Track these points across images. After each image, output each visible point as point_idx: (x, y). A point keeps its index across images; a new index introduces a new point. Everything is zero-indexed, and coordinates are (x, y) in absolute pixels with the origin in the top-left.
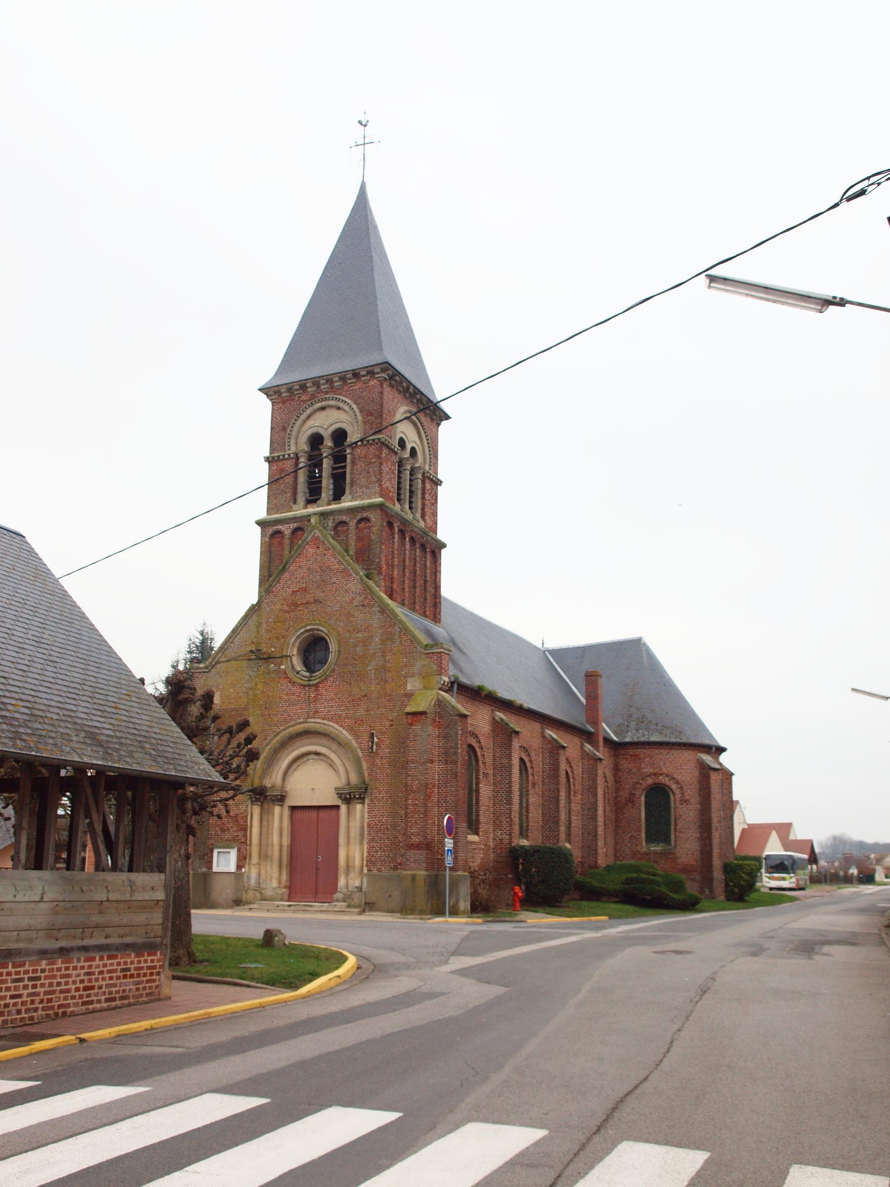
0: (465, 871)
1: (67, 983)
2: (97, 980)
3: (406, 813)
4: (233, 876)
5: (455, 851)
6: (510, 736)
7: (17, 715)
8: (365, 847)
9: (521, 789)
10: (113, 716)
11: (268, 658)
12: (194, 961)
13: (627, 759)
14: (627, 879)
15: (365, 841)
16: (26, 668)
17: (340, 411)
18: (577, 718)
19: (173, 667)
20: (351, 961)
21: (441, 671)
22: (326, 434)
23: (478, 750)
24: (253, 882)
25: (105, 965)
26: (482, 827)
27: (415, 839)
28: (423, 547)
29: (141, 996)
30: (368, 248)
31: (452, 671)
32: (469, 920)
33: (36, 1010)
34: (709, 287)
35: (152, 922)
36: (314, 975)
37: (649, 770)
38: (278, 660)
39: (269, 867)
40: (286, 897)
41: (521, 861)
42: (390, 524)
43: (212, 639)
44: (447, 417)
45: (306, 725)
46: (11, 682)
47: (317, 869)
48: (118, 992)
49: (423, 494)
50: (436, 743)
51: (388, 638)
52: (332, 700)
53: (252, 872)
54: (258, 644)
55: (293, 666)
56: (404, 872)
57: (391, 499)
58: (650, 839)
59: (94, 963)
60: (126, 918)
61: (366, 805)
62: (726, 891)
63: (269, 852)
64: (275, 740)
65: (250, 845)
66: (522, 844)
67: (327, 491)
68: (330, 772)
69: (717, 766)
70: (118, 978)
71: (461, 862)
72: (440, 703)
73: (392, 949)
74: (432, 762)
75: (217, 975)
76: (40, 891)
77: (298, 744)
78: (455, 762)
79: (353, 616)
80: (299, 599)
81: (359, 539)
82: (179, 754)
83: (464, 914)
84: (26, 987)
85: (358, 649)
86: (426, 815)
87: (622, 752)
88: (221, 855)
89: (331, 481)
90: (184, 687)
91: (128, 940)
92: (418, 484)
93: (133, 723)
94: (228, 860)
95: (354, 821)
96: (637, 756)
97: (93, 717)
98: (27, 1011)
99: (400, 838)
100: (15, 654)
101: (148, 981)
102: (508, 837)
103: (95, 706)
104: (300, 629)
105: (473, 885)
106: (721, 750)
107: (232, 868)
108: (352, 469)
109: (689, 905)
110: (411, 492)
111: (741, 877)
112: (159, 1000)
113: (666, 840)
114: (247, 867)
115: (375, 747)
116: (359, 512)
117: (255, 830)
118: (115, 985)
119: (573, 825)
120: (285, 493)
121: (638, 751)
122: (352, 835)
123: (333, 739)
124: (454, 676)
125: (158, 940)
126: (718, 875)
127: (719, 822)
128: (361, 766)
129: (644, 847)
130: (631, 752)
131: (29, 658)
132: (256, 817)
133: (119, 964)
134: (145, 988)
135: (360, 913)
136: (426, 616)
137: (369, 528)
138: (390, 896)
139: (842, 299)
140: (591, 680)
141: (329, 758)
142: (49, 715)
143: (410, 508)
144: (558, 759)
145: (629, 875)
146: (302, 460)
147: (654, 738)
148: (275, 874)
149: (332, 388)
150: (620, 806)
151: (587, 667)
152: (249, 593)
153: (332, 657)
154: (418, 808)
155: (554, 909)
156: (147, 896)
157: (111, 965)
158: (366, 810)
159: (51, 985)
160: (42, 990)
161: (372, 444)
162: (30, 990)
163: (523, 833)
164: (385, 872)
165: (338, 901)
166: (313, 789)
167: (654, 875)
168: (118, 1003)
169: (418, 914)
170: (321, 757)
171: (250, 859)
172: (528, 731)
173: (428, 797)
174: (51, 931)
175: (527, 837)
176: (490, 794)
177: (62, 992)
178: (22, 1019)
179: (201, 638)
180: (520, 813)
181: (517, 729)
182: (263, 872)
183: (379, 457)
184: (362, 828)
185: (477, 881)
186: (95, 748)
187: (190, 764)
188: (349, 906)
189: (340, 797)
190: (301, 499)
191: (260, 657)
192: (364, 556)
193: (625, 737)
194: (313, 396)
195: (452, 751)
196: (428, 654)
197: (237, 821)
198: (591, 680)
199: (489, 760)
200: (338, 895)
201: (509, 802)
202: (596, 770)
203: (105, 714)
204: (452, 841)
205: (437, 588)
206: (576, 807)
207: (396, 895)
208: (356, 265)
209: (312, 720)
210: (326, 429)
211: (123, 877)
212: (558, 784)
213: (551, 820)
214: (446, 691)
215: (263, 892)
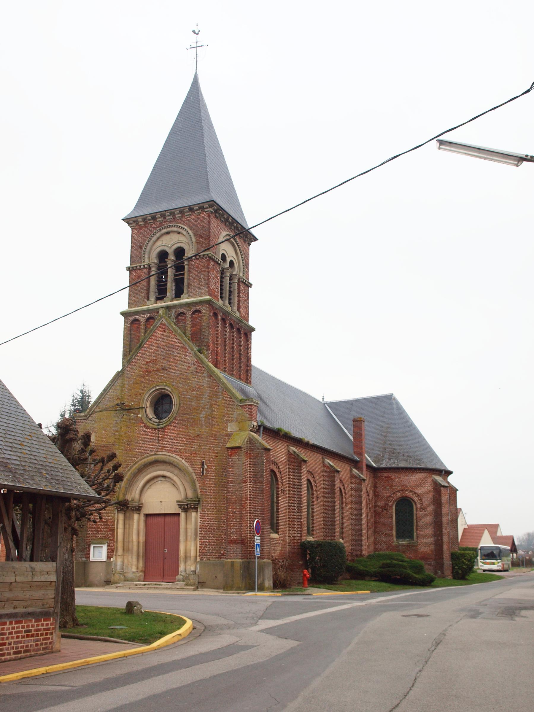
0: (269, 559)
3: (227, 519)
6: (300, 464)
8: (198, 542)
9: (308, 501)
10: (19, 451)
11: (129, 409)
12: (77, 625)
15: (198, 538)
17: (180, 235)
18: (347, 451)
19: (62, 416)
20: (189, 624)
21: (251, 417)
22: (170, 251)
23: (278, 474)
25: (13, 628)
26: (281, 528)
27: (234, 537)
28: (239, 330)
29: (39, 649)
30: (200, 121)
31: (259, 418)
34: (439, 148)
35: (47, 597)
36: (163, 634)
38: (136, 411)
40: (142, 579)
41: (308, 552)
42: (215, 315)
43: (89, 396)
44: (256, 239)
45: (156, 457)
47: (164, 558)
49: (239, 293)
50: (248, 468)
51: (214, 395)
52: (174, 438)
53: (118, 561)
54: (122, 399)
55: (147, 415)
57: (216, 297)
58: (398, 536)
60: (28, 594)
61: (199, 513)
62: (452, 573)
63: (130, 547)
64: (134, 467)
65: (117, 542)
66: (309, 540)
68: (174, 489)
69: (446, 485)
70: (23, 637)
71: (266, 553)
73: (217, 615)
74: (245, 482)
77: (151, 470)
78: (262, 482)
80: (152, 368)
81: (194, 325)
82: (67, 478)
83: (268, 589)
87: (379, 475)
88: (96, 549)
89: (174, 284)
90: (70, 430)
91: (30, 610)
92: (236, 286)
94: (101, 553)
95: (190, 525)
96: (390, 477)
97: (5, 452)
99: (223, 536)
101: (44, 639)
102: (299, 535)
105: (274, 569)
106: (449, 473)
107: (104, 558)
108: (189, 276)
110: (230, 292)
111: (463, 563)
112: (52, 652)
113: (411, 537)
114: (114, 557)
115: (205, 472)
116: (194, 306)
117: (120, 531)
118: (20, 642)
119: (345, 526)
123: (175, 466)
125: (51, 610)
126: (447, 561)
128: (195, 486)
129: (395, 541)
134: (42, 644)
135: (194, 590)
140: (357, 423)
141: (172, 480)
143: (230, 303)
144: (334, 479)
145: (384, 561)
148: (135, 562)
149: (174, 218)
150: (377, 513)
151: (354, 415)
152: (116, 364)
153: (174, 408)
154: (236, 515)
156: (43, 579)
157: (18, 628)
158: (199, 516)
161: (202, 258)
163: (310, 532)
164: (213, 560)
165: (179, 581)
166: (161, 502)
167: (402, 561)
168: (23, 655)
169: (236, 590)
170: (167, 479)
172: (313, 461)
173: (242, 507)
175: (312, 535)
176: (286, 505)
179: (81, 395)
180: (308, 518)
182: (126, 561)
183: (208, 268)
184: (196, 530)
185: (278, 566)
186: (6, 474)
187: (74, 484)
188: (186, 585)
190: (152, 297)
191: (123, 408)
193: (381, 464)
195: (259, 474)
196: (243, 406)
197: (107, 525)
198: (357, 423)
199: (285, 481)
200: (179, 577)
201: (300, 510)
202: (361, 488)
203: (14, 449)
204: (259, 538)
207: (220, 576)
208: (191, 133)
209: (161, 453)
210: (170, 248)
211: (26, 565)
213: (329, 523)
215: (126, 575)
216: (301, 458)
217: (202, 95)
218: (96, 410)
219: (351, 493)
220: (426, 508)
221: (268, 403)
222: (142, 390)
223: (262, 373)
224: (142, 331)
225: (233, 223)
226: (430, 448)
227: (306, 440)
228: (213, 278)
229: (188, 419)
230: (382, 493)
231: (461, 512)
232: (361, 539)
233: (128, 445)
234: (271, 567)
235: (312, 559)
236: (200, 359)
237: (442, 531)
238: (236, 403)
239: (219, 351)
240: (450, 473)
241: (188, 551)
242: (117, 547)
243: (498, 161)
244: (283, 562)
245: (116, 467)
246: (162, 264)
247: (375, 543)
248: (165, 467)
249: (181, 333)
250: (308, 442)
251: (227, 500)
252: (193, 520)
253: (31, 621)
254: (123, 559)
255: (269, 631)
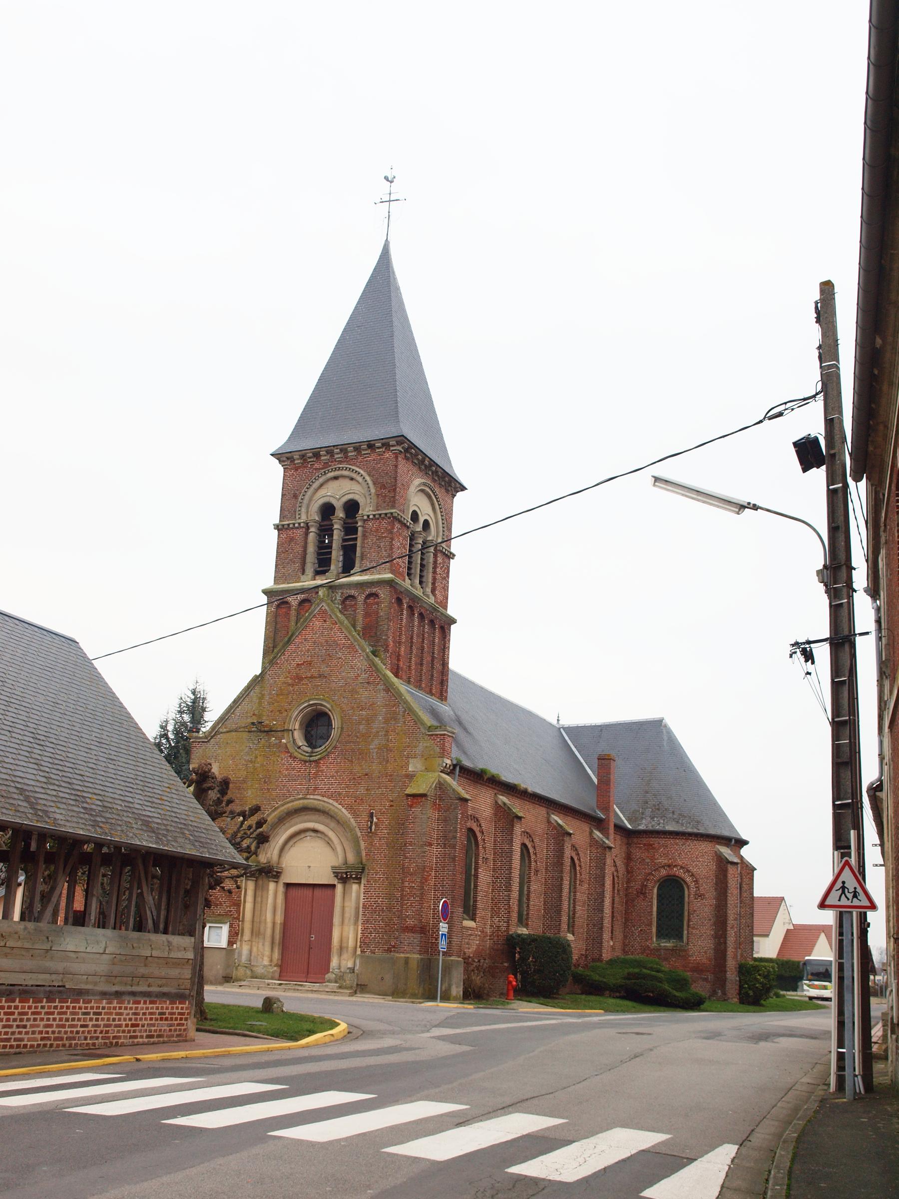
0: (459, 957)
1: (119, 1020)
2: (141, 1019)
3: (402, 895)
4: (224, 951)
5: (450, 936)
6: (513, 821)
7: (94, 807)
8: (360, 927)
9: (521, 877)
10: (160, 806)
11: (269, 731)
12: (206, 1019)
13: (640, 848)
14: (629, 974)
15: (360, 922)
16: (94, 766)
17: (353, 482)
18: (586, 801)
19: (162, 727)
20: (343, 1026)
21: (443, 753)
22: (338, 505)
23: (479, 835)
24: (244, 958)
25: (147, 1008)
26: (480, 913)
27: (410, 922)
28: (432, 622)
29: (173, 1036)
30: (389, 314)
31: (455, 753)
32: (460, 1005)
33: (97, 1038)
34: (654, 485)
35: (183, 977)
36: (311, 1032)
37: (663, 861)
38: (279, 734)
39: (261, 944)
40: (277, 975)
41: (518, 949)
42: (399, 601)
43: (204, 699)
44: (463, 488)
45: (305, 801)
46: (87, 779)
47: (310, 948)
48: (155, 1031)
49: (435, 568)
50: (435, 825)
51: (392, 717)
52: (332, 777)
53: (243, 949)
54: (260, 716)
55: (294, 740)
56: (397, 955)
57: (400, 575)
58: (660, 934)
59: (140, 1006)
60: (163, 972)
61: (362, 885)
62: (739, 994)
63: (262, 929)
64: (273, 815)
65: (243, 921)
66: (519, 932)
67: (336, 565)
68: (328, 850)
69: (736, 860)
70: (157, 1019)
71: (455, 948)
72: (441, 786)
73: (381, 1021)
74: (430, 845)
75: (230, 1028)
76: (103, 945)
77: (296, 820)
78: (454, 847)
79: (357, 692)
80: (304, 673)
81: (367, 615)
82: (211, 839)
83: (455, 999)
84: (91, 1019)
85: (361, 727)
86: (422, 898)
87: (635, 840)
88: (212, 929)
89: (341, 553)
90: (208, 777)
91: (165, 989)
92: (430, 555)
93: (175, 812)
94: (220, 936)
95: (349, 901)
96: (651, 845)
97: (146, 808)
98: (91, 1038)
99: (396, 920)
100: (85, 755)
101: (178, 1025)
102: (505, 924)
103: (147, 799)
104: (303, 703)
105: (466, 970)
106: (742, 843)
107: (224, 944)
108: (363, 543)
109: (694, 1004)
110: (422, 565)
111: (756, 979)
112: (186, 1041)
113: (680, 937)
114: (238, 943)
115: (373, 827)
116: (368, 587)
117: (249, 906)
118: (154, 1025)
119: (577, 915)
120: (294, 562)
121: (652, 840)
122: (347, 915)
123: (332, 817)
124: (456, 759)
125: (187, 992)
126: (732, 975)
127: (735, 919)
128: (359, 846)
129: (654, 942)
130: (645, 841)
131: (95, 757)
132: (250, 893)
133: (157, 1008)
134: (175, 1030)
135: (351, 995)
136: (432, 694)
137: (377, 603)
138: (382, 979)
139: (754, 505)
140: (604, 763)
141: (326, 835)
142: (115, 806)
143: (421, 582)
144: (563, 845)
145: (631, 970)
146: (312, 529)
147: (669, 828)
148: (267, 952)
149: (346, 457)
150: (630, 897)
151: (603, 748)
152: (252, 663)
153: (334, 733)
154: (414, 891)
155: (549, 1000)
156: (180, 955)
157: (152, 1008)
158: (362, 890)
159: (108, 1020)
160: (102, 1023)
161: (383, 519)
162: (94, 1022)
163: (522, 920)
164: (379, 954)
165: (329, 981)
166: (309, 867)
167: (658, 971)
168: (155, 1039)
169: (409, 998)
170: (319, 835)
171: (242, 936)
172: (532, 817)
173: (425, 880)
174: (110, 977)
175: (527, 926)
176: (489, 880)
177: (116, 1026)
178: (88, 1044)
179: (193, 697)
180: (520, 901)
181: (520, 814)
182: (255, 949)
183: (391, 533)
184: (357, 908)
185: (471, 968)
186: (150, 834)
187: (219, 848)
188: (340, 987)
189: (336, 876)
190: (310, 570)
191: (261, 729)
192: (371, 632)
193: (639, 825)
194: (326, 465)
195: (451, 835)
196: (432, 735)
198: (604, 763)
199: (489, 845)
200: (330, 976)
201: (508, 888)
202: (605, 859)
203: (154, 805)
204: (446, 925)
205: (445, 664)
206: (581, 896)
207: (388, 978)
208: (377, 338)
209: (312, 797)
210: (338, 500)
211: (163, 938)
212: (562, 872)
213: (553, 909)
214: (448, 774)
215: (254, 969)
216: (514, 813)
217: (394, 273)
218: (221, 730)
219: (590, 866)
220: (704, 895)
221: (471, 730)
222: (290, 704)
223: (465, 682)
224: (293, 618)
225: (431, 466)
226: (715, 803)
227: (523, 786)
228: (398, 548)
229: (353, 750)
230: (639, 869)
231: (783, 903)
232: (601, 935)
233: (265, 782)
234: (461, 969)
235: (523, 959)
236: (373, 665)
237: (726, 930)
238: (423, 730)
239: (402, 653)
240: (745, 843)
241: (344, 940)
242: (243, 930)
243: (718, 507)
244: (479, 961)
245: (260, 824)
246: (325, 523)
247: (624, 943)
248: (316, 817)
249: (349, 625)
250: (526, 789)
251: (403, 869)
252: (354, 895)
253: (165, 1002)
254: (251, 946)
255: (439, 1038)
